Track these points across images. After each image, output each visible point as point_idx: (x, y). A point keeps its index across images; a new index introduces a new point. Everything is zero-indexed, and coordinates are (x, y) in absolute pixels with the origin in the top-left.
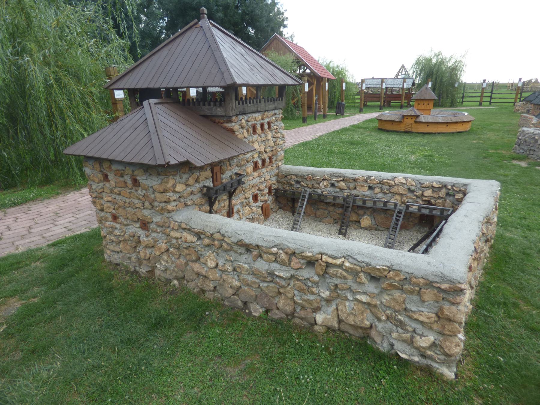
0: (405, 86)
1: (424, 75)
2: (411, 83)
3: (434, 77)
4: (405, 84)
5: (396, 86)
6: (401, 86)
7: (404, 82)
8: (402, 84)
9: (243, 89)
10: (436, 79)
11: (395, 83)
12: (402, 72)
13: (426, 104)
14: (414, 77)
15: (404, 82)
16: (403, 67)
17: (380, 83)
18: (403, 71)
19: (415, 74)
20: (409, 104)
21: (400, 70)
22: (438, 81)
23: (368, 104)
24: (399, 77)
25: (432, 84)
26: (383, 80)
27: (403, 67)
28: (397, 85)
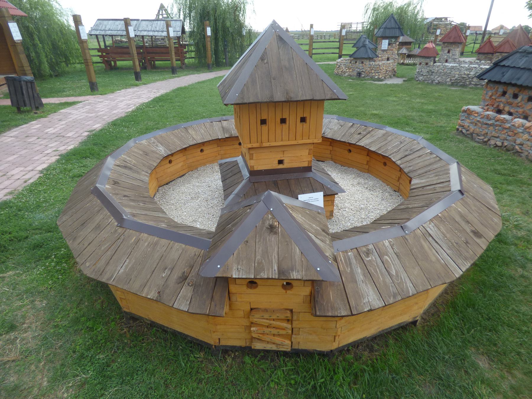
0: (172, 34)
1: (196, 16)
2: (179, 29)
3: (212, 18)
4: (171, 29)
5: (156, 34)
6: (165, 34)
7: (168, 26)
8: (165, 29)
9: (210, 33)
10: (216, 22)
11: (150, 28)
12: (162, 15)
13: (293, 119)
14: (182, 17)
15: (168, 26)
16: (162, 7)
17: (124, 28)
18: (164, 12)
19: (182, 13)
20: (183, 63)
21: (159, 11)
22: (220, 25)
23: (119, 63)
24: (161, 17)
25: (212, 31)
26: (127, 22)
27: (162, 7)
28: (158, 31)
